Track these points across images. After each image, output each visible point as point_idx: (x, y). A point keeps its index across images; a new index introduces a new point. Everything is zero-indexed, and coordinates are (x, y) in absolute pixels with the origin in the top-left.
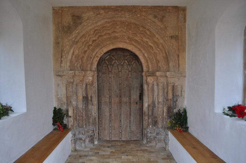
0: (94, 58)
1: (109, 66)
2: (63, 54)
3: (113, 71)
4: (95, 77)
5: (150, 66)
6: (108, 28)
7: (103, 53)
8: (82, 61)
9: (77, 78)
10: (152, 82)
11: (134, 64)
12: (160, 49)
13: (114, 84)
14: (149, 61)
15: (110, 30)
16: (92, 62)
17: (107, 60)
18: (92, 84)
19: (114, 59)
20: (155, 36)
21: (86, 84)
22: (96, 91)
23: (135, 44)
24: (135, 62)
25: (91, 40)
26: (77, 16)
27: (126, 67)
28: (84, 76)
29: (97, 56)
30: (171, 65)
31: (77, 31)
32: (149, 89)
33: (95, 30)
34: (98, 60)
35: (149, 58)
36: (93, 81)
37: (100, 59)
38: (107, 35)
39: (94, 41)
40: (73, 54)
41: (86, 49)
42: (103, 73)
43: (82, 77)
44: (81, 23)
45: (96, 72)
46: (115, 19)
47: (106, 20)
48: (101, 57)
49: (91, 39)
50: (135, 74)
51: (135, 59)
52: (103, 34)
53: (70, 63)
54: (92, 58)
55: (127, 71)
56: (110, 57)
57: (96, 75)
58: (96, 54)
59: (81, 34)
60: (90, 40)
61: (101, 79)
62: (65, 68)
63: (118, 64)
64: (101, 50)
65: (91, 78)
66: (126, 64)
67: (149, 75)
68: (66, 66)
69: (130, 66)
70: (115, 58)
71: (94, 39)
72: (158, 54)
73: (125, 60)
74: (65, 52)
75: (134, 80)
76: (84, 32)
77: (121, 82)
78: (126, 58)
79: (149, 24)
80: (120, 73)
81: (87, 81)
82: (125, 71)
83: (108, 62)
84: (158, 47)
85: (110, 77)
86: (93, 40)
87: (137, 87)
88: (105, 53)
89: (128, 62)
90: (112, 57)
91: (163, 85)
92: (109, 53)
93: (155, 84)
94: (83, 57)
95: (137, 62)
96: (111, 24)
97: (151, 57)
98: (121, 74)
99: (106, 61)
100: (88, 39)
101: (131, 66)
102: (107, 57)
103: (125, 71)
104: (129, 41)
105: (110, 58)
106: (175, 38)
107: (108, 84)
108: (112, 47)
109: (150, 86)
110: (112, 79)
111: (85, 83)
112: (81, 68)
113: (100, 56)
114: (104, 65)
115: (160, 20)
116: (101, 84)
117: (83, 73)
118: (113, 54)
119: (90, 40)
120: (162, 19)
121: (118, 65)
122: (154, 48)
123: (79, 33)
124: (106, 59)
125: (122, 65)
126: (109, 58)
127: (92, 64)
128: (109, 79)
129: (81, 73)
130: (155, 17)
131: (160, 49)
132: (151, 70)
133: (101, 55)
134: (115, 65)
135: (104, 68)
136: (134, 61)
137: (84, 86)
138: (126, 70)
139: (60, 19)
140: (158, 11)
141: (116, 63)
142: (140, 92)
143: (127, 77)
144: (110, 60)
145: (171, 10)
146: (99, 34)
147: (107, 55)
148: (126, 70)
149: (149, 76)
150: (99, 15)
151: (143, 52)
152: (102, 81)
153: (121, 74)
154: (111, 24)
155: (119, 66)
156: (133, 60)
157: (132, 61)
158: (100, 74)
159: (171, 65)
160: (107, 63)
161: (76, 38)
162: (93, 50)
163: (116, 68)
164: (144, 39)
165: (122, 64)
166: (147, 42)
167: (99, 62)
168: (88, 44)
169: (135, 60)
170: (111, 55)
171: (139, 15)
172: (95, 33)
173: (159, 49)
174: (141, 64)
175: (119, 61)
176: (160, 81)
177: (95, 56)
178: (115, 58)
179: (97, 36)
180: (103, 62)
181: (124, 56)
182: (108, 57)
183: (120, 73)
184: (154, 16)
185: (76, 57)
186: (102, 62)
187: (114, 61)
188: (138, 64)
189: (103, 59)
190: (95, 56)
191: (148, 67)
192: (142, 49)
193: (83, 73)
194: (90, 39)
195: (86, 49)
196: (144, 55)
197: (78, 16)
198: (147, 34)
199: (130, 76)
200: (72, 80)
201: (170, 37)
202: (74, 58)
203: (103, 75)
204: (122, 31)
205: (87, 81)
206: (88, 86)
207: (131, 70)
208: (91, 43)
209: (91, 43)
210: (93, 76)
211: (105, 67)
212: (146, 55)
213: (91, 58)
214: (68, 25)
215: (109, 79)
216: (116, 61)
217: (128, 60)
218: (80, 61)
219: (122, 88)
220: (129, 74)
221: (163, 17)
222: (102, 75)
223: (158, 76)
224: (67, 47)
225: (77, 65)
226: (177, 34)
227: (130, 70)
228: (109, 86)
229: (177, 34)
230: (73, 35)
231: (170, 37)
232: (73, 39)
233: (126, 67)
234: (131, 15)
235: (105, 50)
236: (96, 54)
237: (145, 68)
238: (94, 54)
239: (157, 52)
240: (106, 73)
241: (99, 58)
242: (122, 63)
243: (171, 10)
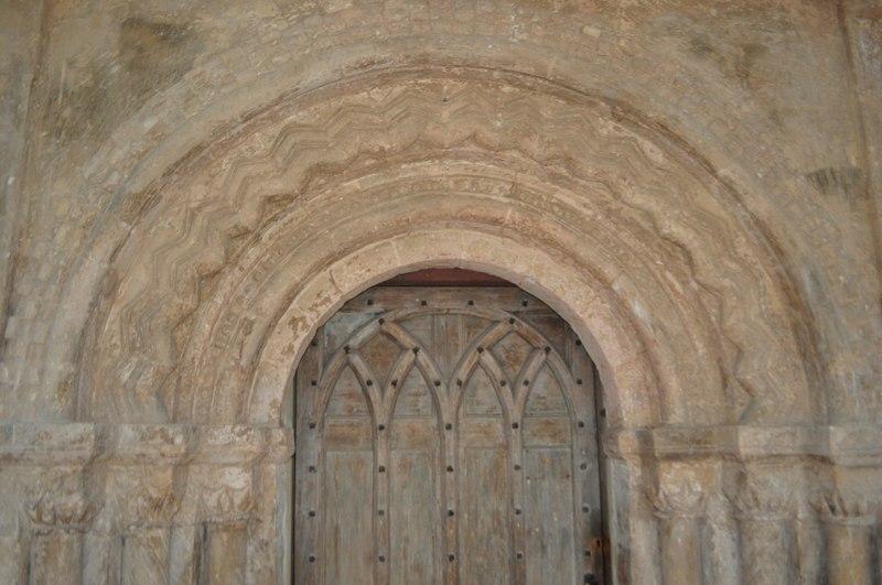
0: (270, 328)
1: (374, 391)
2: (23, 287)
3: (401, 426)
4: (277, 470)
5: (673, 384)
6: (377, 119)
7: (336, 299)
8: (177, 350)
9: (124, 478)
10: (691, 500)
11: (543, 377)
12: (740, 261)
13: (407, 512)
14: (662, 353)
15: (393, 131)
16: (254, 363)
17: (360, 350)
18: (244, 528)
19: (407, 341)
20: (713, 172)
21: (204, 524)
22: (279, 561)
23: (560, 235)
24: (546, 362)
25: (249, 195)
26: (157, 27)
27: (485, 395)
28: (182, 466)
29: (294, 322)
30: (848, 376)
31: (149, 124)
32: (672, 552)
33: (286, 133)
34: (297, 344)
35: (662, 328)
36: (252, 504)
37: (314, 343)
38: (370, 170)
39: (275, 203)
40: (108, 287)
41: (214, 257)
42: (337, 440)
43: (166, 477)
44: (179, 73)
45: (279, 435)
46: (430, 49)
47: (366, 53)
48: (320, 330)
49: (254, 189)
50: (547, 441)
51: (543, 342)
52: (341, 156)
53: (77, 357)
54: (258, 329)
55: (498, 426)
56: (382, 333)
57: (283, 452)
58: (289, 299)
59: (177, 146)
60: (242, 194)
61: (317, 477)
62: (33, 397)
63: (434, 374)
64: (324, 274)
65: (238, 480)
66: (484, 379)
67: (670, 449)
68: (35, 379)
69: (513, 389)
70: (412, 337)
71: (277, 187)
72: (731, 301)
73: (480, 350)
74: (43, 274)
75: (546, 484)
76: (197, 132)
77: (458, 502)
78: (490, 337)
79: (663, 92)
80: (450, 435)
81: (212, 501)
82: (484, 422)
83: (371, 366)
84: (728, 247)
85: (382, 469)
86: (270, 199)
87: (565, 534)
88: (348, 306)
89: (501, 364)
90: (394, 329)
91: (789, 526)
92: (377, 307)
93: (718, 512)
94: (187, 318)
95: (558, 364)
96: (398, 90)
97: (674, 327)
98: (457, 446)
99: (356, 359)
100: (234, 188)
101: (523, 389)
102: (360, 328)
103: (484, 422)
104: (517, 216)
105: (382, 338)
106: (846, 187)
107: (368, 513)
108: (397, 258)
109: (680, 532)
110: (397, 479)
111: (189, 516)
112: (162, 405)
113: (312, 320)
114: (343, 386)
115: (731, 67)
116: (318, 518)
117: (179, 440)
118: (401, 314)
119: (242, 194)
120: (748, 65)
121: (438, 384)
122: (700, 256)
123: (158, 136)
124: (353, 343)
125: (459, 383)
126: (373, 337)
127: (251, 372)
128: (375, 480)
129: (158, 440)
130: (701, 48)
131: (740, 261)
132: (677, 416)
133: (323, 310)
134: (417, 383)
135: (340, 405)
136: (539, 358)
137: (185, 542)
138: (488, 414)
139: (35, 37)
140: (714, 12)
141: (420, 367)
142: (590, 571)
143: (497, 466)
144: (385, 347)
145: (794, 13)
146: (312, 158)
147: (360, 318)
148: (488, 414)
149: (673, 457)
150: (315, 20)
151: (616, 287)
152: (326, 493)
153: (457, 446)
154: (398, 90)
155: (442, 388)
156: (535, 349)
157: (529, 359)
158: (314, 445)
159: (848, 376)
160: (365, 373)
161: (134, 171)
162: (264, 274)
163: (424, 402)
164: (627, 193)
165: (462, 374)
166: (648, 215)
167: (304, 358)
168: (227, 225)
169: (547, 350)
170: (389, 317)
171: (592, 31)
172: (287, 147)
173: (733, 266)
174: (593, 380)
175: (441, 361)
176: (763, 495)
177: (277, 317)
178: (420, 342)
179: (297, 172)
180: (337, 362)
181: (474, 325)
182: (369, 330)
183: (450, 435)
184: (695, 42)
185: (128, 318)
186: (325, 366)
187: (408, 358)
188: (566, 377)
189: (338, 342)
190: (277, 317)
191: (657, 394)
192: (609, 271)
193: (179, 440)
194: (245, 184)
195: (214, 257)
196: (621, 309)
197: (167, 27)
198: (648, 163)
199: (516, 457)
200: (76, 501)
201: (808, 176)
202: (116, 327)
203: (329, 454)
204: (473, 138)
205: (212, 501)
206: (219, 546)
207: (525, 415)
208: (254, 216)
209: (247, 216)
210: (256, 465)
211: (351, 395)
212: (638, 309)
213: (248, 327)
214: (87, 81)
215: (375, 480)
216: (422, 356)
217: (499, 350)
218: (162, 347)
219: (462, 542)
220: (507, 447)
221: (752, 50)
222: (324, 451)
223: (749, 459)
224: (62, 233)
225: (135, 376)
226: (854, 163)
227: (515, 416)
228: (374, 529)
229: (854, 163)
230: (114, 146)
231: (808, 176)
232: (115, 177)
233: (485, 395)
234: (539, 31)
235: (352, 277)
236: (289, 299)
237: (628, 405)
238: (270, 301)
239: (727, 282)
240: (354, 441)
241: (303, 335)
242: (462, 374)
243: (794, 13)
